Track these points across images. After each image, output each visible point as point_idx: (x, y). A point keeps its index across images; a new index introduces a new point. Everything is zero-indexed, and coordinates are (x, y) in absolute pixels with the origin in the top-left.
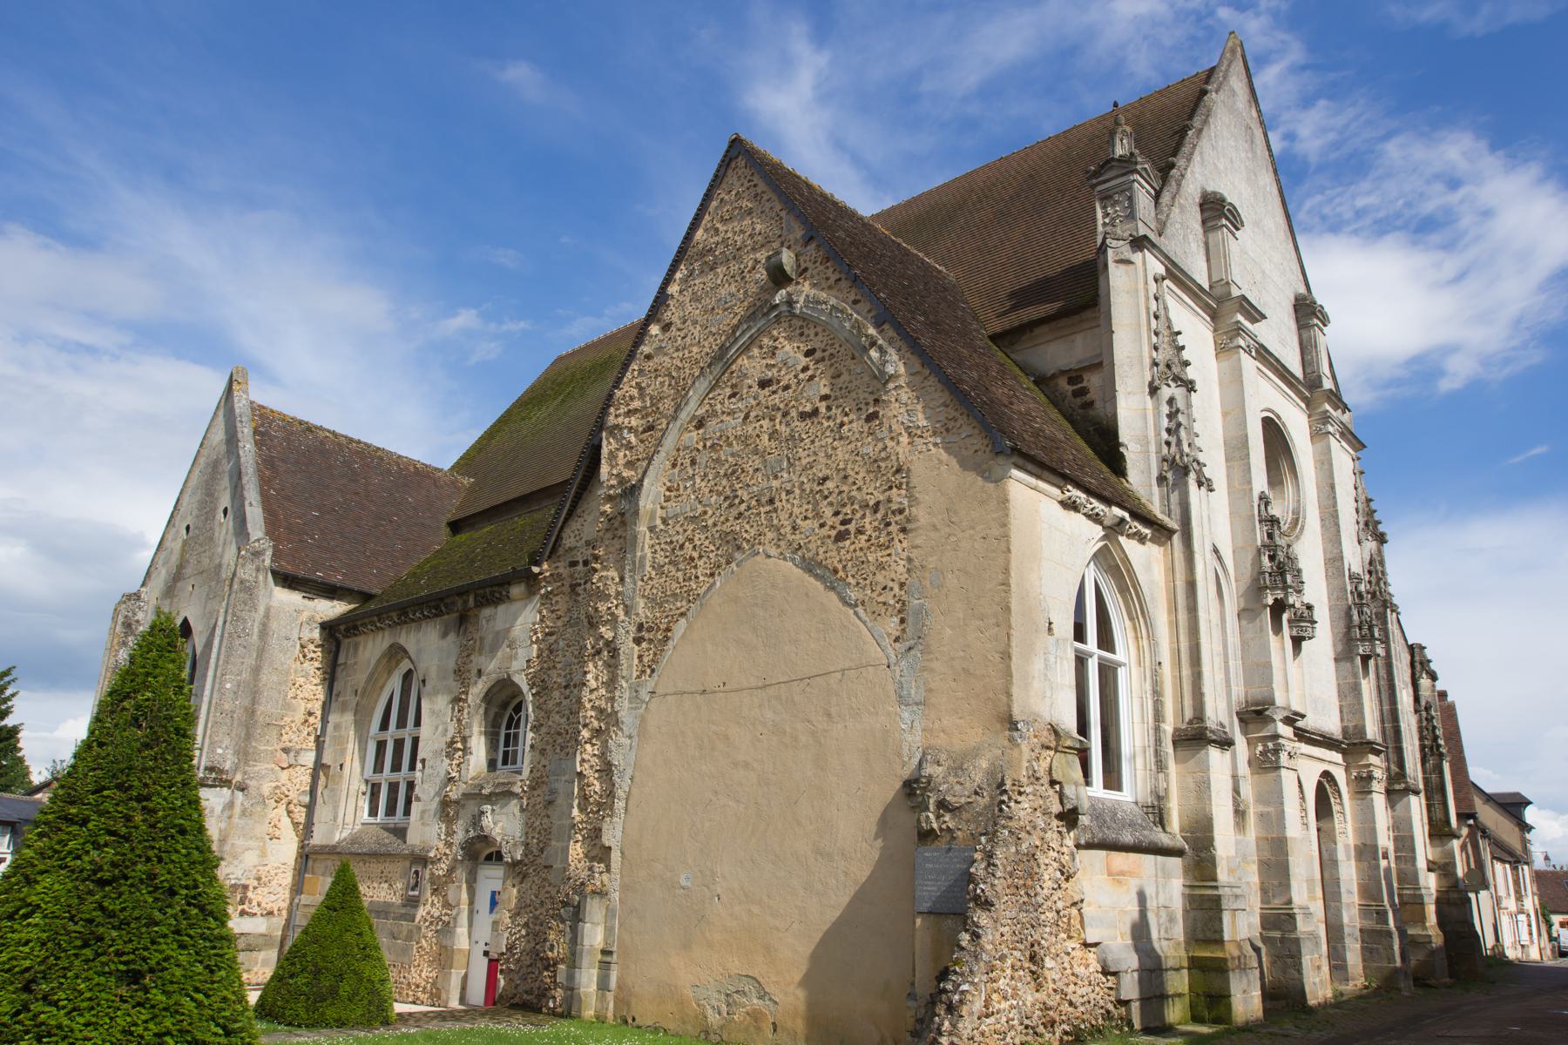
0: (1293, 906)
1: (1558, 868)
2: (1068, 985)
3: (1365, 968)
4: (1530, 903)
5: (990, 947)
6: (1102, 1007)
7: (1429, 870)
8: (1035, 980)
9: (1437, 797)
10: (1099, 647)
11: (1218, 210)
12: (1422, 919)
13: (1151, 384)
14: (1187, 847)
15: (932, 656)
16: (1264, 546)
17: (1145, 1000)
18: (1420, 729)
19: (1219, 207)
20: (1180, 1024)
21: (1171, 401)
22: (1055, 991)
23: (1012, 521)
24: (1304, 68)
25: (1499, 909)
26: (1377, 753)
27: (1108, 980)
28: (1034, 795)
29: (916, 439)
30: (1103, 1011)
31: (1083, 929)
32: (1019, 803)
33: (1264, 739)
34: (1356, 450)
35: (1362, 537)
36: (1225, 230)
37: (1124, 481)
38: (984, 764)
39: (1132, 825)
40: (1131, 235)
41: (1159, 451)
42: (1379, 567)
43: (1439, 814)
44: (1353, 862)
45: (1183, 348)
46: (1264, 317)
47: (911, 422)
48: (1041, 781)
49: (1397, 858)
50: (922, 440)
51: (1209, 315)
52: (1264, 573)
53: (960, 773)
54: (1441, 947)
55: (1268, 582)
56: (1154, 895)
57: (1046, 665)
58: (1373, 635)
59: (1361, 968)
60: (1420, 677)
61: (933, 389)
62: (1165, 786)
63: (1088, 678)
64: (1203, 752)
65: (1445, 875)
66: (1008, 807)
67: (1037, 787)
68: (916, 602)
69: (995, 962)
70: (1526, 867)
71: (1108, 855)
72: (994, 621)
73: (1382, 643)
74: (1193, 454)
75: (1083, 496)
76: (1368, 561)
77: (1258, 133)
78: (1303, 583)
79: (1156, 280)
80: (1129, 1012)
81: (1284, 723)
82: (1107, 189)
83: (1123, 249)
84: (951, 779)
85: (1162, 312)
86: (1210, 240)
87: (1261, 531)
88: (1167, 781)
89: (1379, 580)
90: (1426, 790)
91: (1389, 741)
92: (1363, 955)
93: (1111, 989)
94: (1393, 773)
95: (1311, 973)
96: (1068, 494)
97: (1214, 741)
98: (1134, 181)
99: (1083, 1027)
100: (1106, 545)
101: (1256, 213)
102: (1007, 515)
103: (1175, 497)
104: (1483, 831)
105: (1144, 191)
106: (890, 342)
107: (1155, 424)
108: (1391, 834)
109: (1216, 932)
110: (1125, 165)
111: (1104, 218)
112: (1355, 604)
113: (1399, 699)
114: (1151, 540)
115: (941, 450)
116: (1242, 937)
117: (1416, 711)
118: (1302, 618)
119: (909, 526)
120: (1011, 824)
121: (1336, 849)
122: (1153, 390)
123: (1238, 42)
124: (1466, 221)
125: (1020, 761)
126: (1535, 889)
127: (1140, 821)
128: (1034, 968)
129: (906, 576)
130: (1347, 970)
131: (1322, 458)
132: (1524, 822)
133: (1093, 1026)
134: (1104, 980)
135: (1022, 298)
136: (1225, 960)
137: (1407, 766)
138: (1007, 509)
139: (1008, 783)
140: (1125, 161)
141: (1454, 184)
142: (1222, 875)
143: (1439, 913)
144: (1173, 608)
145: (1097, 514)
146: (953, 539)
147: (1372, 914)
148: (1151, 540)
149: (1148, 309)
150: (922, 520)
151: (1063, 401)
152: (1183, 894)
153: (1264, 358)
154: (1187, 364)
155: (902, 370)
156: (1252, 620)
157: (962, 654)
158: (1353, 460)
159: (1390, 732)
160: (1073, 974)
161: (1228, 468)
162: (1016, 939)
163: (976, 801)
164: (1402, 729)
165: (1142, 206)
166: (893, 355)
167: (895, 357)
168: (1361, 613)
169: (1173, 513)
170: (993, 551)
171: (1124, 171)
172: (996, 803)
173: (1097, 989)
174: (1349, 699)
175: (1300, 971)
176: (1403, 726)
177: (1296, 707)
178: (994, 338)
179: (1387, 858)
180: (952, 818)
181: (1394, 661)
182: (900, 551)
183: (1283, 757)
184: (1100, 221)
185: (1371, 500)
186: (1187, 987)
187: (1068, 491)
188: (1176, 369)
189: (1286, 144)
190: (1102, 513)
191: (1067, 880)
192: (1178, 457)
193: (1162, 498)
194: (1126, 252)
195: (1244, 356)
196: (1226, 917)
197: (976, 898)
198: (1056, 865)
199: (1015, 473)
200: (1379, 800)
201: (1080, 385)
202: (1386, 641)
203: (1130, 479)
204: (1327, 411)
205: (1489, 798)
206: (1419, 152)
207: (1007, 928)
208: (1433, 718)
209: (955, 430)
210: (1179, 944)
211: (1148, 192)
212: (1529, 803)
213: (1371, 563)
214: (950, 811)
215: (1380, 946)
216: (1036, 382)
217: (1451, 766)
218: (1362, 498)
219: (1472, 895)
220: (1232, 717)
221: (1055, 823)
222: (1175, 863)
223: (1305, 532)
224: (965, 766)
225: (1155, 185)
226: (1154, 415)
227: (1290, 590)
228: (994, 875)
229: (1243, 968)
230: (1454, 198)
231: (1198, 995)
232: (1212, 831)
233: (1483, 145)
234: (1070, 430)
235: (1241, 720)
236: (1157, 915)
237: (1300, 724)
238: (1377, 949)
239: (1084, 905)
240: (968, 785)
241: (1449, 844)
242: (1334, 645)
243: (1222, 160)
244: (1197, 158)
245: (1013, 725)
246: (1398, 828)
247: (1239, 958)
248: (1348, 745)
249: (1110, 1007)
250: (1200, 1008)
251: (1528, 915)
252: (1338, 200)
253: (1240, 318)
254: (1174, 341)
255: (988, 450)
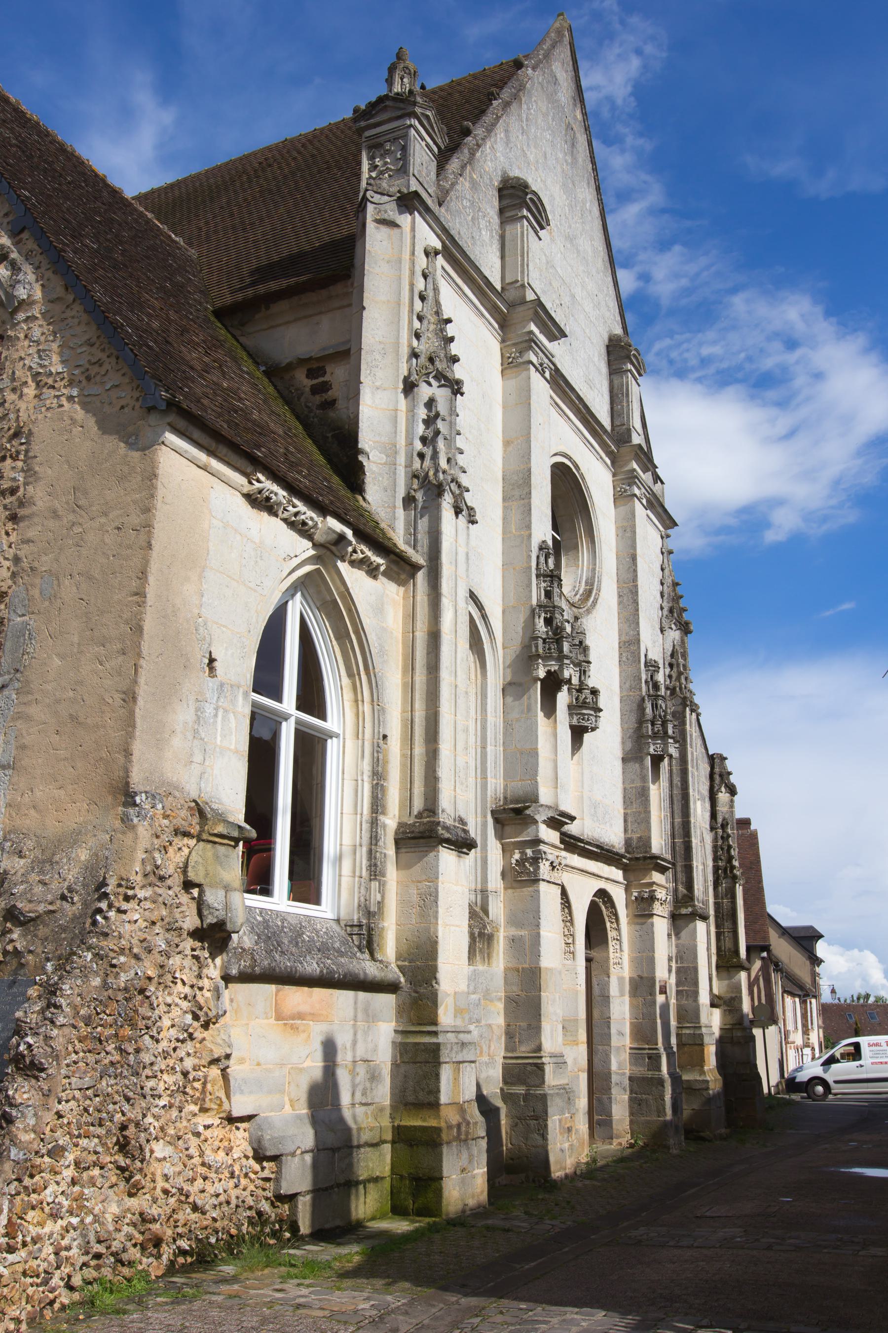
0: (543, 1054)
1: (842, 1001)
2: (192, 1180)
3: (631, 1122)
4: (815, 1037)
5: (26, 1137)
6: (250, 1208)
7: (713, 1005)
8: (128, 1180)
9: (728, 924)
10: (298, 708)
11: (521, 198)
12: (700, 1061)
13: (406, 380)
14: (402, 980)
15: (30, 697)
16: (540, 606)
17: (319, 1192)
18: (715, 849)
19: (520, 194)
20: (373, 1219)
21: (430, 403)
22: (166, 1192)
23: (159, 505)
24: (663, 211)
25: (787, 1043)
26: (662, 870)
27: (263, 1169)
28: (154, 902)
29: (45, 390)
30: (253, 1213)
31: (228, 1097)
32: (125, 912)
33: (522, 845)
34: (666, 527)
35: (666, 624)
36: (526, 223)
37: (360, 498)
38: (83, 855)
39: (324, 949)
40: (399, 192)
41: (409, 465)
42: (681, 660)
43: (728, 944)
44: (627, 998)
45: (452, 339)
46: (564, 335)
47: (41, 366)
48: (169, 882)
49: (678, 993)
50: (53, 392)
51: (497, 322)
52: (536, 638)
53: (48, 867)
54: (719, 1093)
55: (541, 651)
56: (349, 1045)
57: (198, 718)
58: (666, 732)
59: (628, 1123)
60: (719, 790)
61: (76, 321)
62: (379, 898)
63: (279, 748)
64: (432, 854)
65: (730, 1011)
66: (106, 918)
67: (160, 891)
68: (19, 619)
69: (38, 1161)
70: (814, 1001)
71: (278, 991)
72: (119, 646)
73: (676, 742)
74: (452, 472)
75: (282, 493)
76: (669, 653)
77: (582, 139)
78: (589, 662)
79: (427, 253)
80: (294, 1210)
81: (548, 826)
82: (377, 136)
83: (387, 206)
84: (34, 877)
85: (430, 294)
86: (508, 233)
87: (538, 588)
88: (382, 890)
89: (680, 674)
90: (717, 917)
91: (678, 859)
92: (630, 1107)
93: (267, 1180)
94: (680, 896)
95: (559, 1137)
96: (257, 485)
97: (447, 841)
98: (411, 126)
99: (213, 1240)
100: (318, 570)
101: (570, 227)
102: (152, 496)
103: (423, 524)
104: (776, 965)
105: (423, 144)
106: (28, 257)
107: (407, 431)
108: (674, 965)
109: (430, 1092)
110: (402, 105)
111: (370, 171)
112: (649, 696)
113: (692, 811)
114: (385, 574)
115: (77, 407)
116: (467, 1098)
117: (712, 828)
118: (584, 705)
119: (21, 512)
120: (104, 943)
121: (608, 983)
122: (409, 387)
123: (566, 25)
124: (800, 381)
125: (133, 850)
126: (820, 1023)
127: (337, 945)
128: (122, 1161)
129: (10, 582)
130: (612, 1127)
131: (625, 524)
132: (816, 956)
133: (232, 1236)
134: (257, 1167)
135: (264, 273)
136: (438, 1130)
137: (696, 887)
138: (153, 487)
139: (112, 882)
140: (402, 101)
141: (791, 344)
142: (446, 1017)
143: (721, 1055)
144: (410, 667)
145: (304, 523)
146: (77, 529)
147: (643, 1059)
148: (385, 574)
149: (412, 286)
150: (40, 503)
151: (299, 399)
152: (393, 1043)
153: (564, 392)
154: (455, 359)
155: (38, 294)
156: (518, 697)
157: (71, 694)
158: (662, 538)
159: (680, 848)
160: (203, 1164)
161: (505, 509)
162: (90, 1119)
163: (61, 909)
164: (694, 845)
165: (418, 161)
166: (28, 274)
167: (31, 277)
168: (655, 706)
169: (419, 544)
170: (129, 547)
171: (400, 113)
172: (90, 912)
173: (244, 1182)
174: (634, 806)
175: (544, 1136)
176: (695, 841)
177: (567, 806)
178: (221, 314)
179: (665, 993)
180: (23, 935)
181: (690, 768)
182: (5, 547)
183: (544, 868)
184: (365, 175)
185: (677, 584)
186: (388, 1168)
187: (258, 481)
188: (440, 365)
189: (641, 284)
190: (310, 523)
191: (206, 1026)
192: (431, 473)
193: (407, 523)
194: (391, 211)
195: (535, 376)
196: (446, 1074)
197: (18, 1059)
198: (185, 1005)
199: (170, 437)
200: (661, 926)
201: (321, 379)
202: (682, 740)
203: (367, 497)
204: (634, 470)
205: (785, 932)
206: (762, 309)
207: (72, 1103)
208: (729, 836)
209: (98, 378)
210: (382, 1110)
211: (428, 145)
212: (820, 936)
213: (672, 656)
214: (21, 924)
215: (651, 1097)
216: (268, 374)
217: (744, 890)
218: (668, 581)
219: (757, 1032)
220: (485, 817)
221: (188, 944)
222: (386, 1002)
223: (598, 606)
224: (57, 858)
225: (439, 141)
226: (407, 419)
227: (566, 661)
228: (52, 1022)
229: (463, 1138)
230: (791, 358)
231: (402, 1177)
232: (435, 959)
233: (819, 310)
234: (298, 429)
235: (497, 821)
236: (353, 1073)
237: (573, 828)
238: (647, 1100)
239: (232, 1062)
240: (54, 886)
241: (737, 977)
242: (623, 743)
243: (533, 150)
244: (500, 132)
245: (128, 797)
246: (681, 958)
247: (459, 1126)
248: (629, 859)
249: (265, 1206)
250: (403, 1196)
251: (813, 1049)
252: (685, 346)
253: (533, 327)
254: (442, 330)
255: (138, 405)
